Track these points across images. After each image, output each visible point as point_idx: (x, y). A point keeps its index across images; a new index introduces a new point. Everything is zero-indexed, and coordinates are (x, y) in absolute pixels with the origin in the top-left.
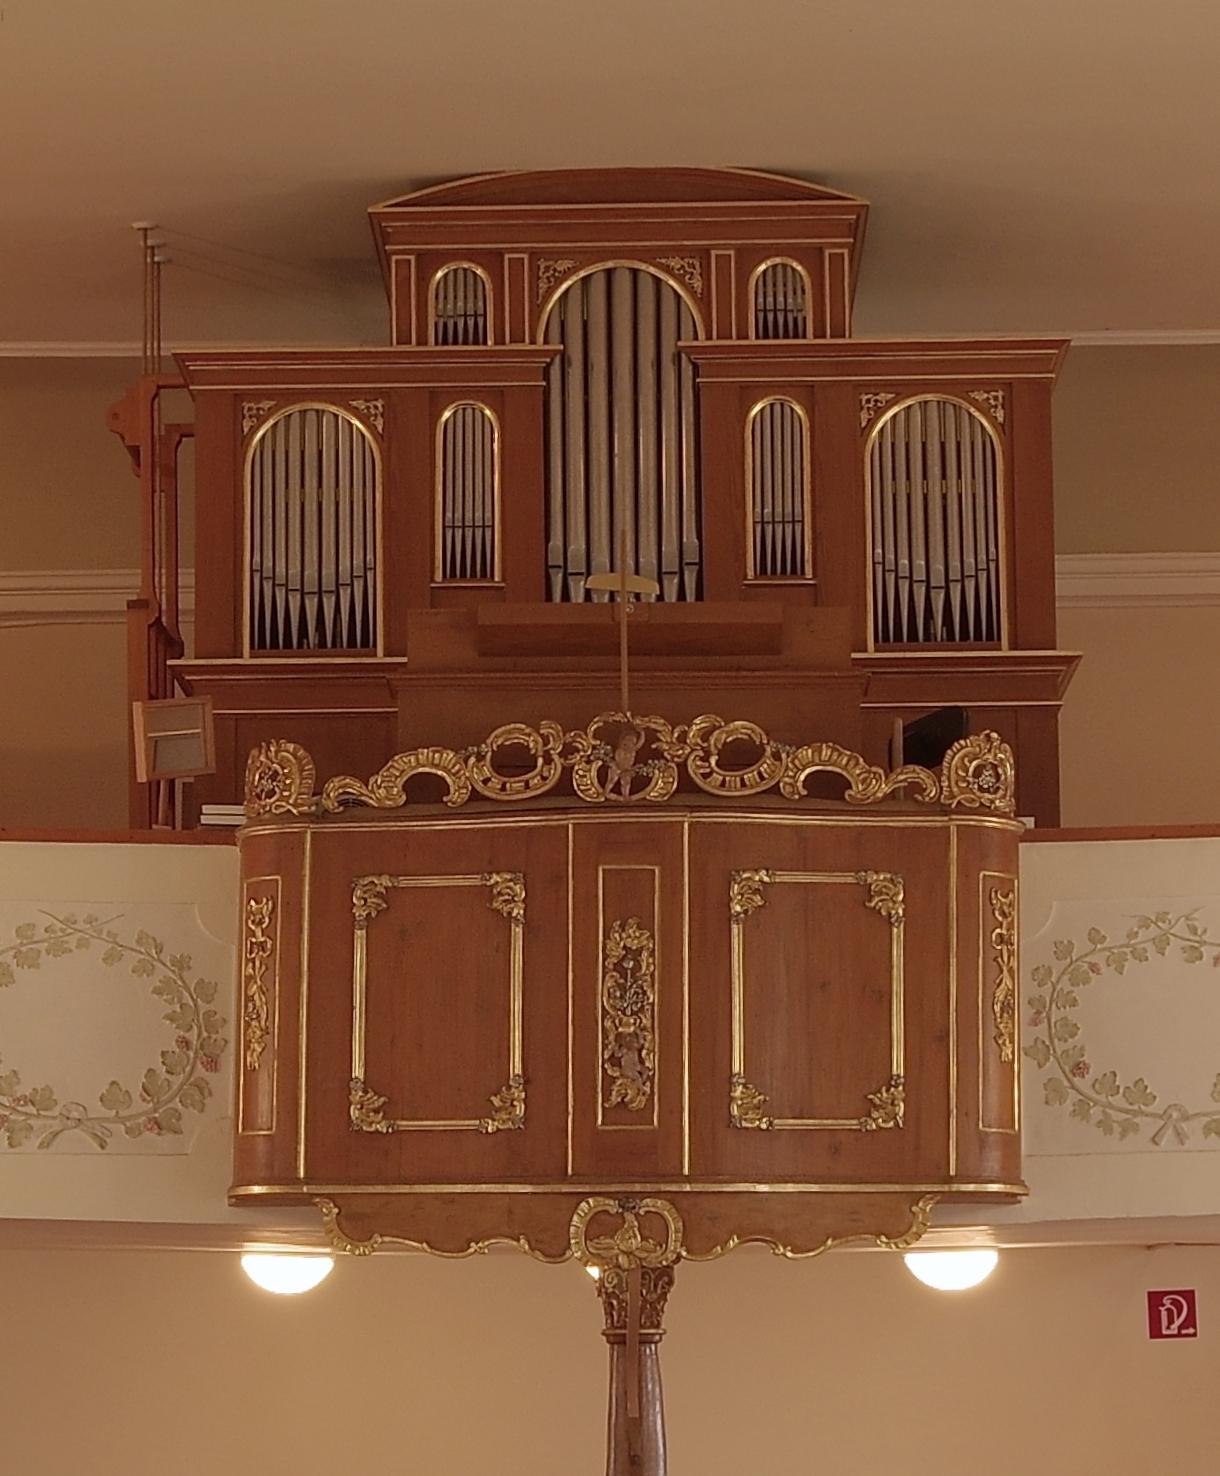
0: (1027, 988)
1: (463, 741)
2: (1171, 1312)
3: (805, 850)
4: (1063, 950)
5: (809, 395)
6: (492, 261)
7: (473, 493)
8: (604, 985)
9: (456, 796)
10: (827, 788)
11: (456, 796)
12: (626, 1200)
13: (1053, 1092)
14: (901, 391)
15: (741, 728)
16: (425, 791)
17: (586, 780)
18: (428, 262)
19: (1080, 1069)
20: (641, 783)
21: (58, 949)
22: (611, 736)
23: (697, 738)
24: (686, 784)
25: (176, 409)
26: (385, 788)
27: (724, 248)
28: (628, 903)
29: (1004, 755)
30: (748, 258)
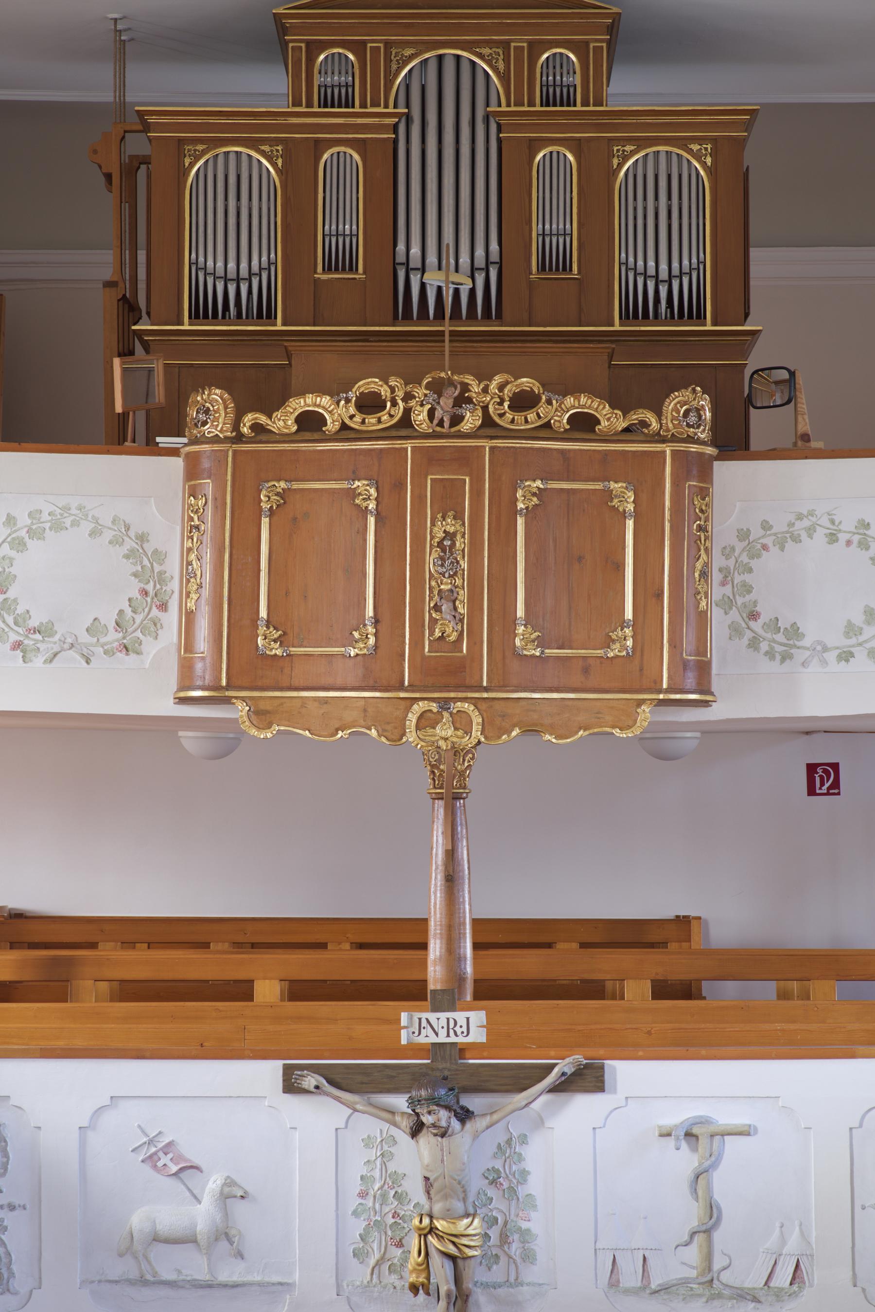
0: (718, 561)
1: (336, 390)
2: (822, 778)
3: (568, 466)
4: (743, 535)
5: (577, 147)
6: (359, 48)
7: (343, 218)
8: (431, 558)
9: (332, 426)
10: (583, 424)
11: (332, 426)
12: (445, 704)
13: (735, 631)
14: (641, 142)
15: (526, 382)
16: (310, 422)
17: (420, 417)
18: (314, 48)
19: (754, 616)
20: (457, 420)
21: (57, 527)
22: (437, 388)
23: (493, 391)
24: (488, 422)
25: (137, 145)
26: (284, 421)
27: (520, 41)
28: (448, 501)
29: (705, 402)
30: (535, 48)
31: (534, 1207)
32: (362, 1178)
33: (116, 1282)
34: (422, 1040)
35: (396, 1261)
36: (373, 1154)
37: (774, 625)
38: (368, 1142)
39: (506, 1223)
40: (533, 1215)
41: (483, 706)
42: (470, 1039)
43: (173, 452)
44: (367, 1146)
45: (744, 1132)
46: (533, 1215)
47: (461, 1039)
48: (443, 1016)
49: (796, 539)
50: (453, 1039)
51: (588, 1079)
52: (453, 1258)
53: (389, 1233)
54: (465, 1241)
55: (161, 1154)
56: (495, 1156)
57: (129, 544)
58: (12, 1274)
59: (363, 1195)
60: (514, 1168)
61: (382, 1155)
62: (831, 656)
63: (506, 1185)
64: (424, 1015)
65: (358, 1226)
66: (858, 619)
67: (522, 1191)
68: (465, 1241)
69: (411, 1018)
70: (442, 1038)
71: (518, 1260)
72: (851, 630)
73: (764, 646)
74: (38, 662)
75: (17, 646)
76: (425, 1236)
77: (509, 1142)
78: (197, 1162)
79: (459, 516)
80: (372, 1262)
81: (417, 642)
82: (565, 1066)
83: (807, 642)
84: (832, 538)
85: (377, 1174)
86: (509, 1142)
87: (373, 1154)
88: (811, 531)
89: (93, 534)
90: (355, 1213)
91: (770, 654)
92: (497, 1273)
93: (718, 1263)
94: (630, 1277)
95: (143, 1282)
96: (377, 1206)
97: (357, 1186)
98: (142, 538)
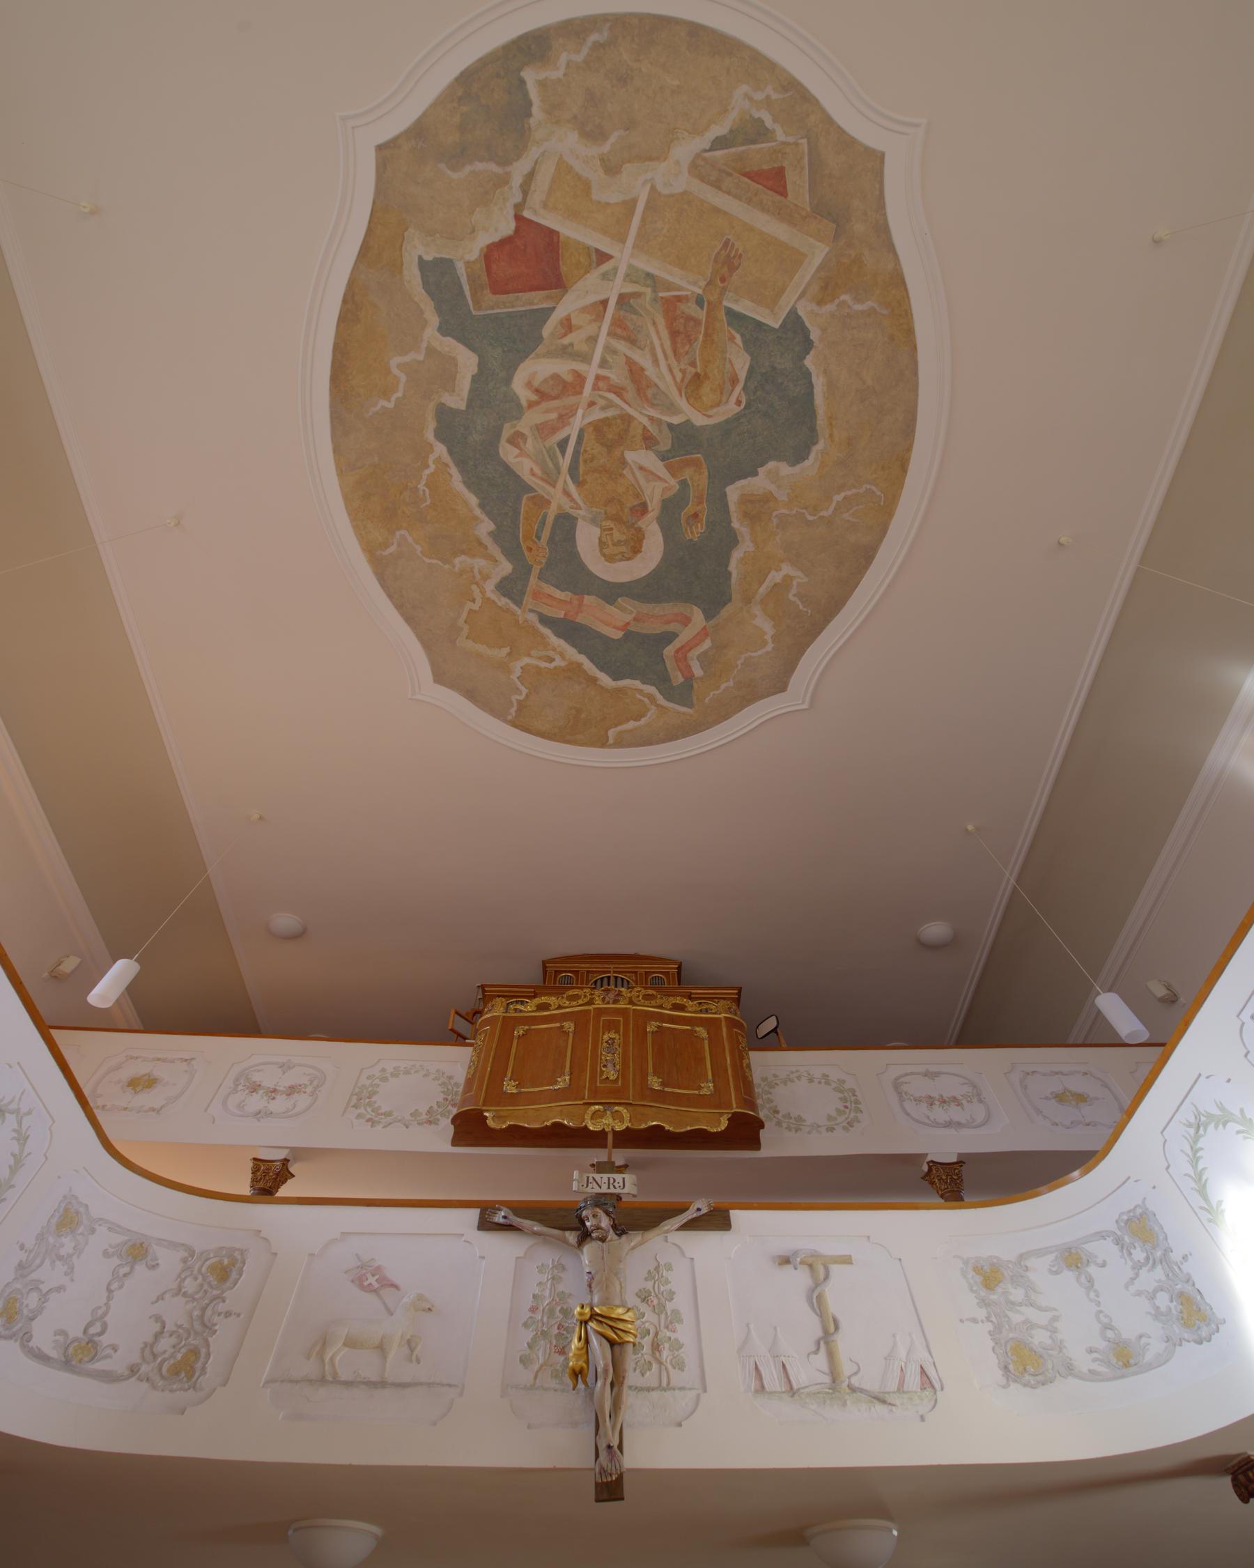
19: (777, 1112)
31: (680, 1321)
32: (534, 1296)
33: (297, 1382)
34: (589, 1190)
35: (558, 1367)
36: (544, 1278)
37: (788, 1116)
38: (541, 1269)
39: (656, 1334)
40: (678, 1326)
41: (631, 1108)
42: (626, 1191)
43: (471, 1045)
44: (540, 1272)
45: (847, 1260)
46: (678, 1326)
47: (618, 1191)
48: (605, 1176)
49: (792, 1081)
50: (612, 1190)
51: (717, 1220)
52: (612, 1343)
53: (554, 1342)
54: (621, 1325)
55: (369, 1275)
56: (646, 1279)
57: (442, 1079)
58: (203, 1369)
59: (533, 1310)
60: (662, 1288)
61: (553, 1278)
62: (823, 1129)
63: (656, 1302)
64: (591, 1175)
65: (528, 1335)
66: (834, 1114)
67: (669, 1306)
68: (621, 1325)
69: (581, 1176)
70: (604, 1190)
71: (670, 1367)
72: (830, 1118)
73: (785, 1125)
74: (379, 1127)
75: (368, 1120)
76: (586, 1322)
77: (657, 1269)
78: (397, 1281)
79: (617, 1032)
80: (536, 1367)
81: (593, 1078)
82: (701, 1205)
83: (808, 1123)
84: (811, 1080)
85: (547, 1293)
86: (657, 1269)
87: (544, 1278)
88: (799, 1078)
89: (425, 1076)
90: (526, 1325)
91: (789, 1128)
92: (651, 1378)
93: (846, 1368)
94: (772, 1379)
95: (322, 1380)
96: (545, 1319)
97: (529, 1302)
98: (450, 1078)
